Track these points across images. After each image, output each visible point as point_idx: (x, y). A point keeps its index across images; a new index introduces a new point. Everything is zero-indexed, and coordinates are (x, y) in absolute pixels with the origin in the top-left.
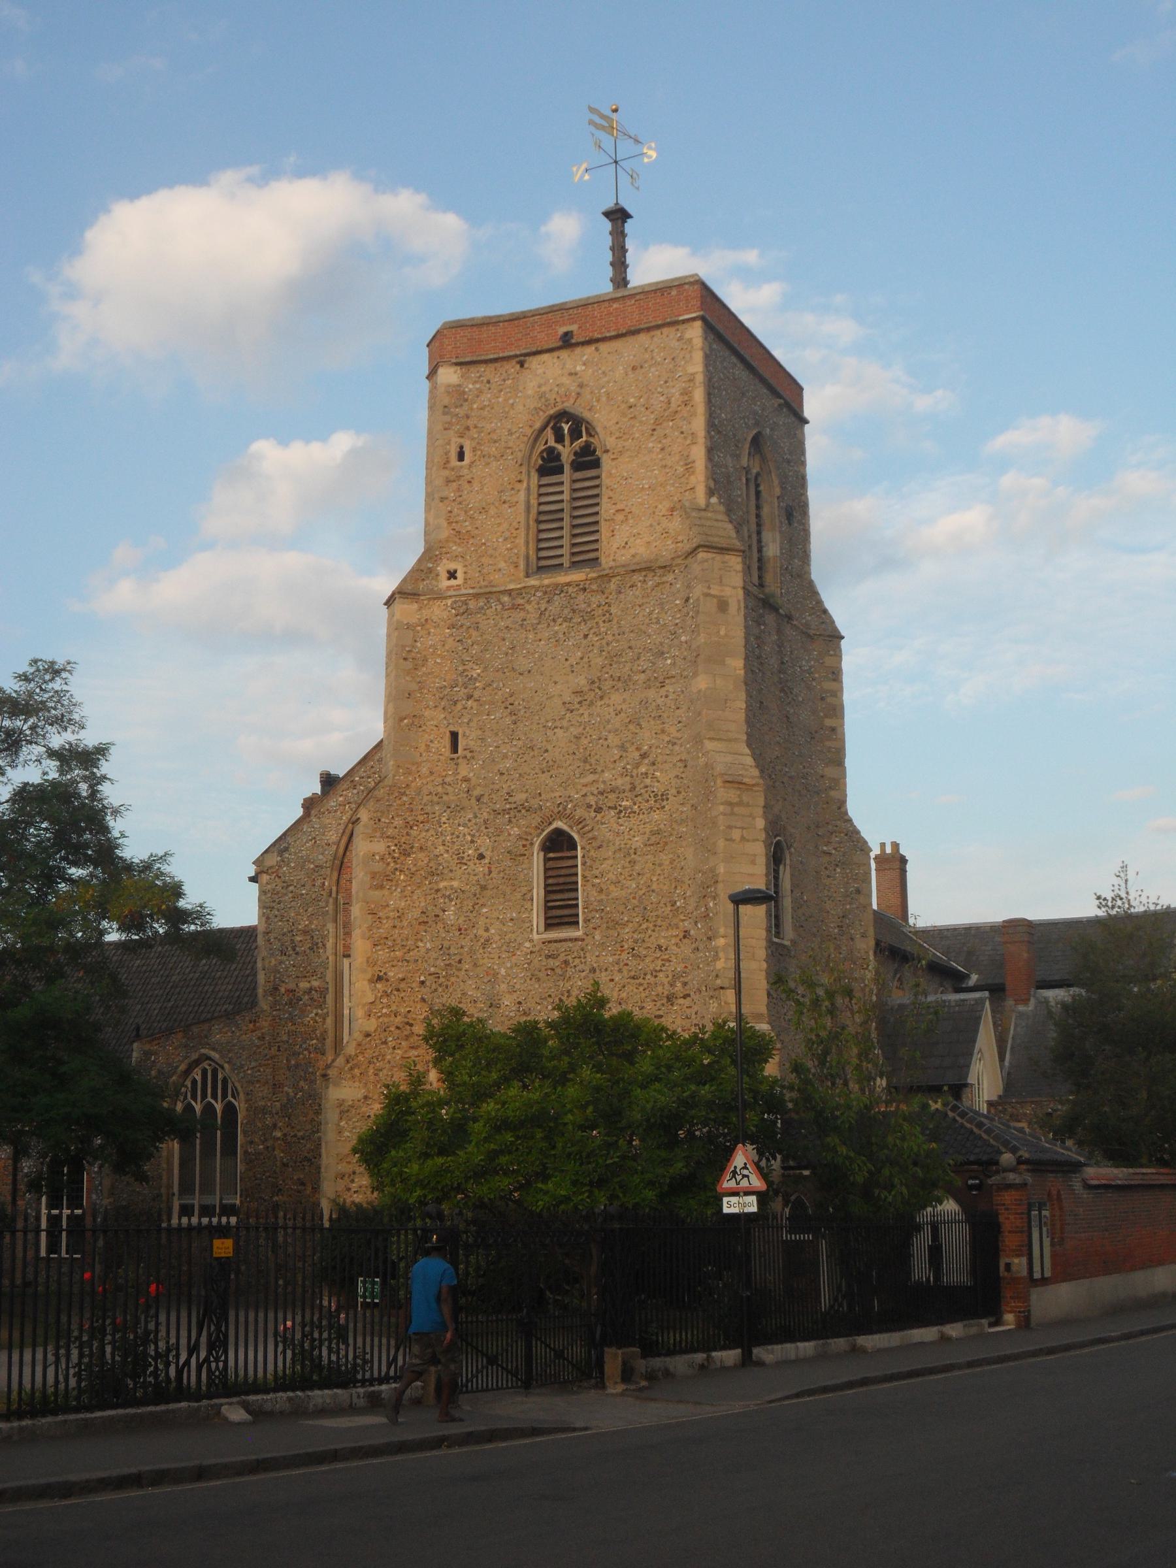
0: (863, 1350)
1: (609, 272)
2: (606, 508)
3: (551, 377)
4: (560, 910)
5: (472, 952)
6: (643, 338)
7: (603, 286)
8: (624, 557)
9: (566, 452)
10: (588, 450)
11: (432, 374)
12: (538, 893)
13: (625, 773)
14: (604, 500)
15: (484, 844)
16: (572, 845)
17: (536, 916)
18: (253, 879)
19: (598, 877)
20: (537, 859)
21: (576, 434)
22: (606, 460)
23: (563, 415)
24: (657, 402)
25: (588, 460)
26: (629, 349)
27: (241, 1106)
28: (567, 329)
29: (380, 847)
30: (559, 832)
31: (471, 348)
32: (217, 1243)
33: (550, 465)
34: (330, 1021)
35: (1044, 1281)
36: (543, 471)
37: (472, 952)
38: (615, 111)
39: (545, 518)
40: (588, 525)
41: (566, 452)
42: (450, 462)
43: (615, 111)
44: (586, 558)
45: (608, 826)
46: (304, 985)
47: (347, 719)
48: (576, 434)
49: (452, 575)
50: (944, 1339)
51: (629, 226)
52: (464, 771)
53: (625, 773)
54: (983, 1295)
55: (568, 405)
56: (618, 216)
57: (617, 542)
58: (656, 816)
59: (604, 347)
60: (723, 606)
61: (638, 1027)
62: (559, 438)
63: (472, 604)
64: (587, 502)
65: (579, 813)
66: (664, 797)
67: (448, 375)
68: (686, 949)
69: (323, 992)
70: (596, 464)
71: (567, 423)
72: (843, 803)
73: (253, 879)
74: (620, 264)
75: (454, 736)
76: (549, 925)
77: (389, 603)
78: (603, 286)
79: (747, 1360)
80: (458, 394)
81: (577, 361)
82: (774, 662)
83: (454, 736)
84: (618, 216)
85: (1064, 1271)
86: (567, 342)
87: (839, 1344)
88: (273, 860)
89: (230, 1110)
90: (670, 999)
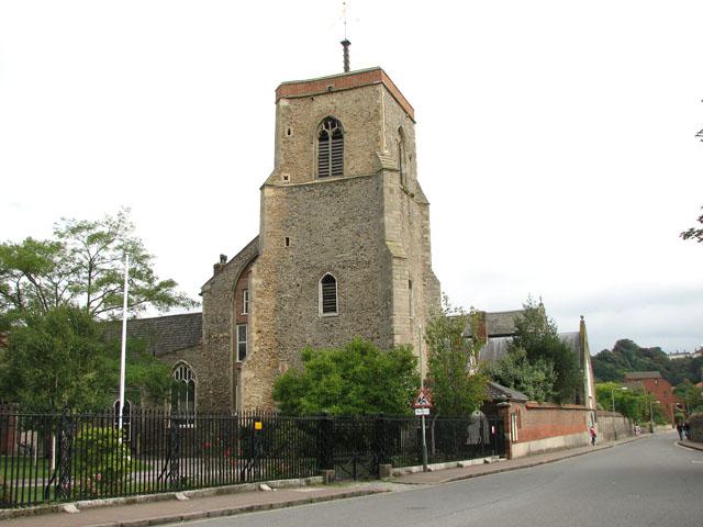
0: (461, 466)
1: (343, 65)
2: (346, 154)
3: (324, 105)
4: (330, 305)
5: (295, 321)
6: (360, 90)
7: (341, 71)
8: (353, 173)
9: (330, 132)
10: (338, 132)
11: (277, 102)
12: (321, 299)
13: (355, 254)
14: (345, 151)
15: (299, 280)
16: (334, 281)
17: (321, 310)
18: (200, 295)
19: (342, 293)
20: (320, 286)
21: (333, 126)
22: (345, 137)
23: (329, 118)
24: (365, 114)
25: (338, 135)
26: (354, 94)
27: (196, 382)
28: (328, 86)
29: (260, 281)
30: (328, 276)
31: (293, 94)
32: (257, 424)
33: (323, 137)
34: (231, 350)
35: (516, 442)
36: (320, 140)
37: (295, 321)
38: (358, 20)
39: (323, 157)
40: (339, 160)
41: (330, 132)
42: (283, 137)
43: (358, 20)
44: (338, 171)
45: (348, 274)
46: (221, 335)
47: (239, 226)
48: (333, 126)
49: (286, 178)
50: (486, 462)
51: (349, 48)
52: (291, 253)
53: (355, 254)
54: (500, 446)
55: (343, 120)
56: (346, 44)
57: (352, 163)
58: (366, 270)
59: (345, 93)
60: (391, 191)
61: (563, 345)
62: (327, 127)
63: (294, 190)
64: (339, 151)
65: (336, 269)
66: (369, 263)
67: (284, 103)
68: (378, 320)
69: (229, 338)
70: (341, 137)
71: (331, 121)
72: (430, 266)
73: (200, 295)
74: (346, 62)
75: (288, 239)
76: (325, 310)
77: (262, 188)
78: (341, 71)
79: (425, 470)
80: (287, 108)
81: (334, 98)
82: (407, 213)
83: (288, 239)
84: (346, 44)
85: (521, 441)
86: (330, 92)
87: (453, 464)
88: (209, 287)
89: (192, 383)
90: (372, 339)
